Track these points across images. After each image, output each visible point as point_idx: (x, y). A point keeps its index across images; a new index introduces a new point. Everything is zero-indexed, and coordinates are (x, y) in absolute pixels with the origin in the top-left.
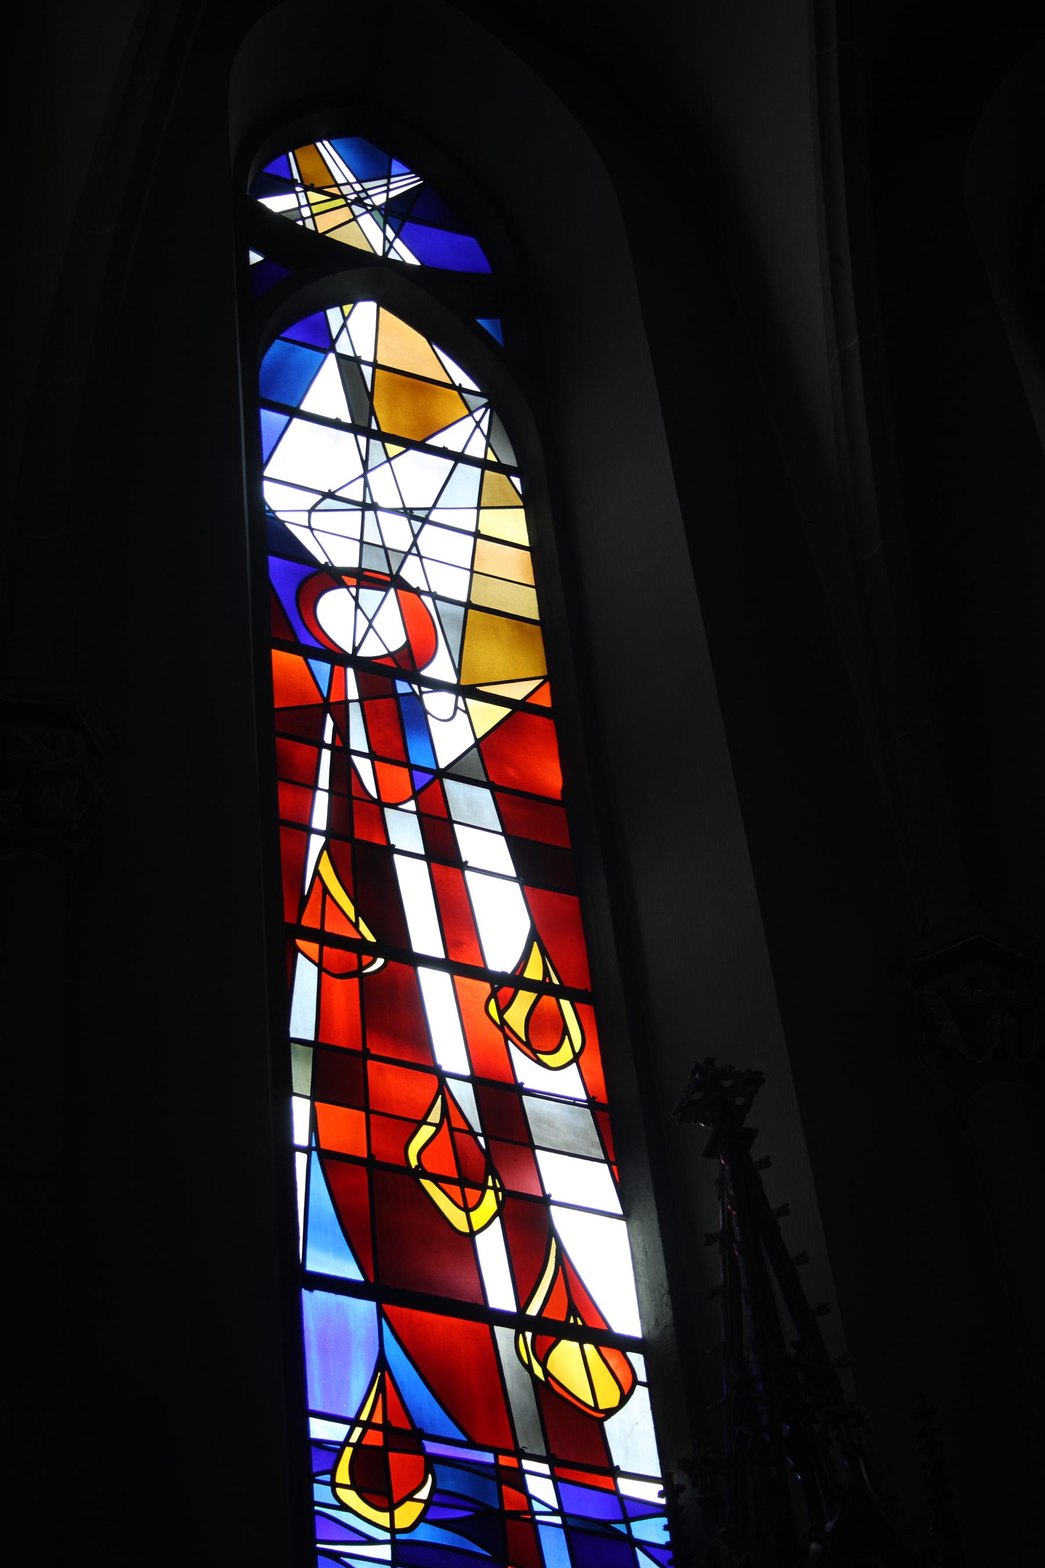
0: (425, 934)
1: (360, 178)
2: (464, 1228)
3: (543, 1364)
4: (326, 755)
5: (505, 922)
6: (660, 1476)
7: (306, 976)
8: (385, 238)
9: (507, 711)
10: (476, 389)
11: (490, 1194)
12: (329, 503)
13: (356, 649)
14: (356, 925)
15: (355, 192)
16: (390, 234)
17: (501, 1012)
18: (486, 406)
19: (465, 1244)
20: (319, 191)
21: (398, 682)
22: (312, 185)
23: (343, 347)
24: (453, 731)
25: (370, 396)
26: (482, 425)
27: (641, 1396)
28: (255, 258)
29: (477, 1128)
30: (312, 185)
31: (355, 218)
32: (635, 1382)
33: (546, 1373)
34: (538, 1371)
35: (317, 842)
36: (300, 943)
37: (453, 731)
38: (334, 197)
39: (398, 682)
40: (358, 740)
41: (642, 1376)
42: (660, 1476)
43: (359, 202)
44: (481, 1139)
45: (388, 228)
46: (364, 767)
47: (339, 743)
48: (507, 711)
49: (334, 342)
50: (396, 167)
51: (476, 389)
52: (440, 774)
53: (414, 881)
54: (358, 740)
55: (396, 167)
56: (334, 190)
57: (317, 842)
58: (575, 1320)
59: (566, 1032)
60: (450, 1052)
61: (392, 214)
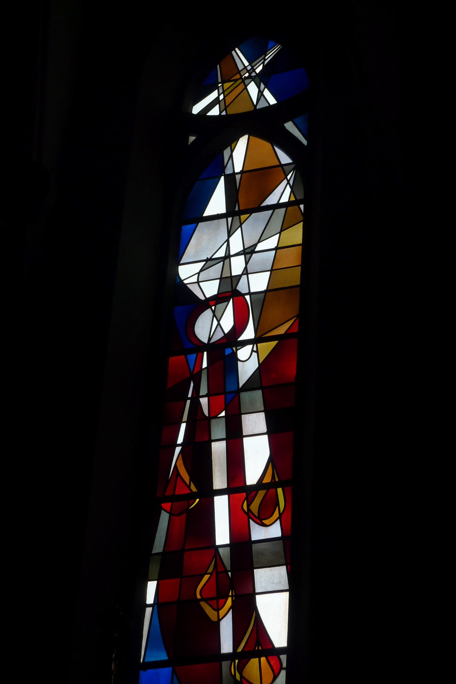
0: (220, 480)
2: (214, 619)
3: (241, 673)
4: (188, 402)
5: (257, 455)
7: (164, 518)
9: (205, 215)
10: (249, 215)
11: (230, 600)
12: (210, 263)
13: (210, 339)
14: (189, 486)
16: (262, 86)
17: (248, 506)
18: (293, 169)
19: (215, 628)
23: (228, 171)
24: (248, 362)
25: (237, 191)
26: (209, 262)
27: (283, 674)
28: (192, 139)
29: (229, 568)
32: (281, 668)
33: (241, 676)
34: (238, 677)
35: (178, 450)
36: (163, 505)
37: (248, 362)
38: (236, 80)
40: (204, 390)
41: (284, 665)
44: (230, 573)
46: (204, 401)
47: (214, 302)
48: (205, 215)
49: (224, 167)
51: (249, 215)
52: (240, 390)
53: (219, 449)
54: (204, 390)
57: (178, 450)
58: (258, 648)
59: (278, 504)
60: (222, 536)
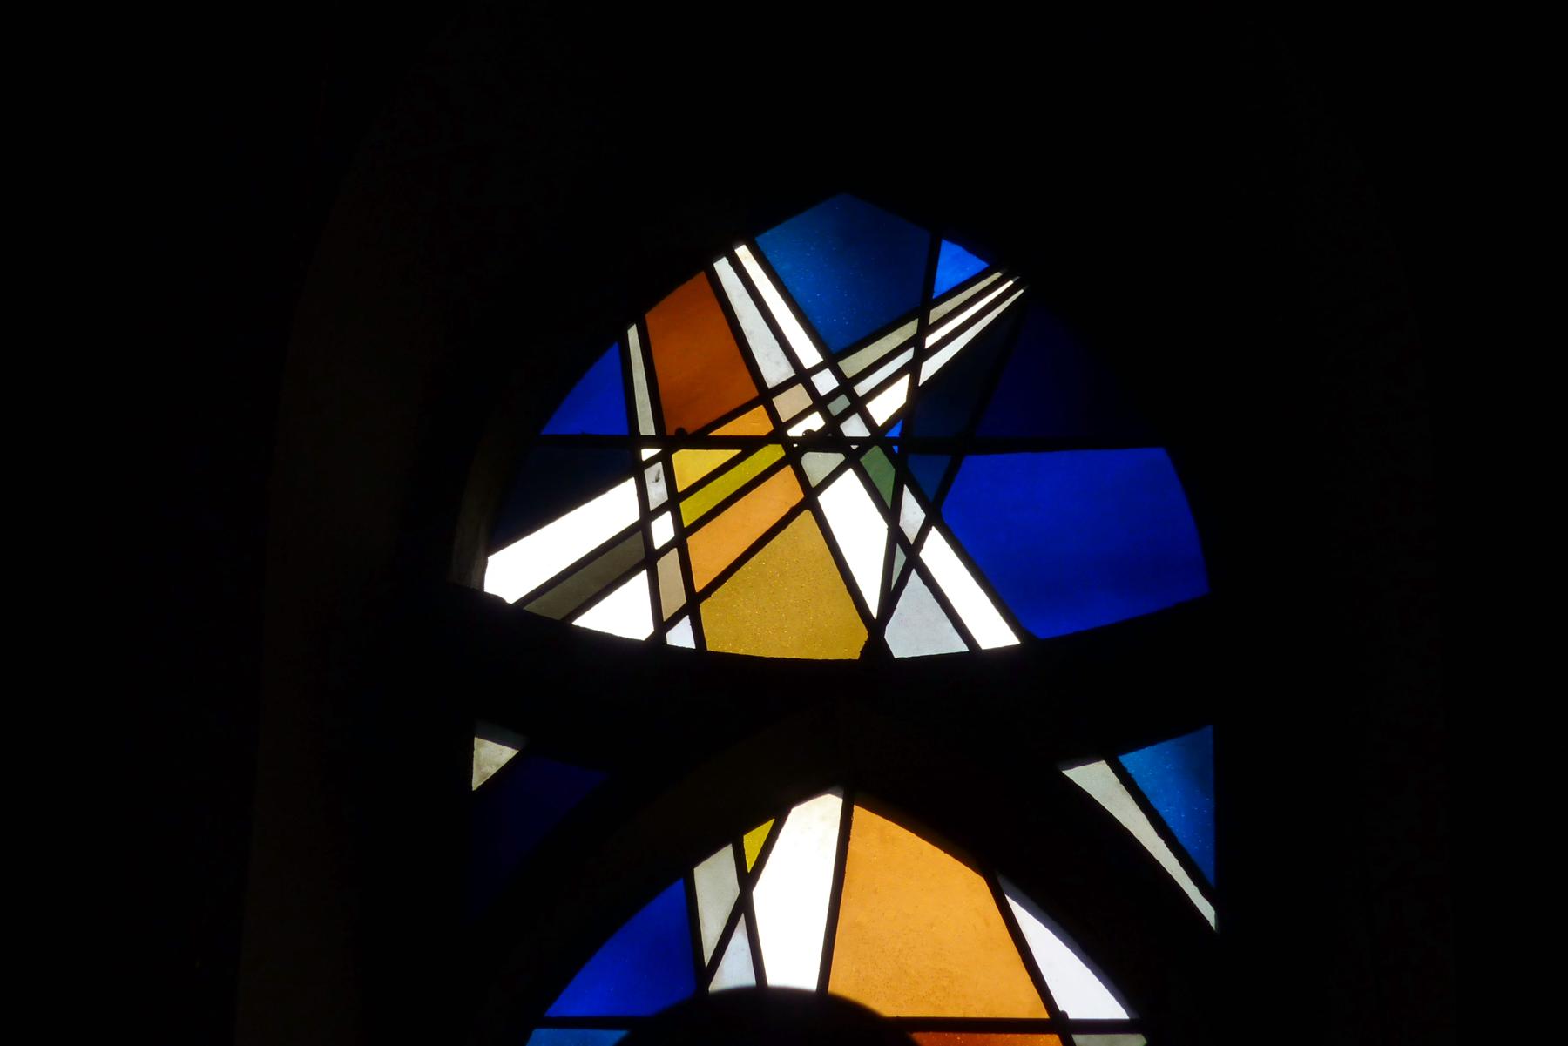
1: (835, 347)
6: (632, 481)
8: (896, 536)
15: (820, 403)
16: (912, 514)
20: (701, 440)
21: (1209, 729)
22: (680, 431)
28: (491, 756)
30: (680, 431)
31: (810, 500)
38: (749, 445)
39: (1209, 729)
42: (632, 481)
43: (829, 439)
45: (909, 500)
50: (953, 262)
55: (953, 262)
56: (754, 423)
61: (927, 457)
